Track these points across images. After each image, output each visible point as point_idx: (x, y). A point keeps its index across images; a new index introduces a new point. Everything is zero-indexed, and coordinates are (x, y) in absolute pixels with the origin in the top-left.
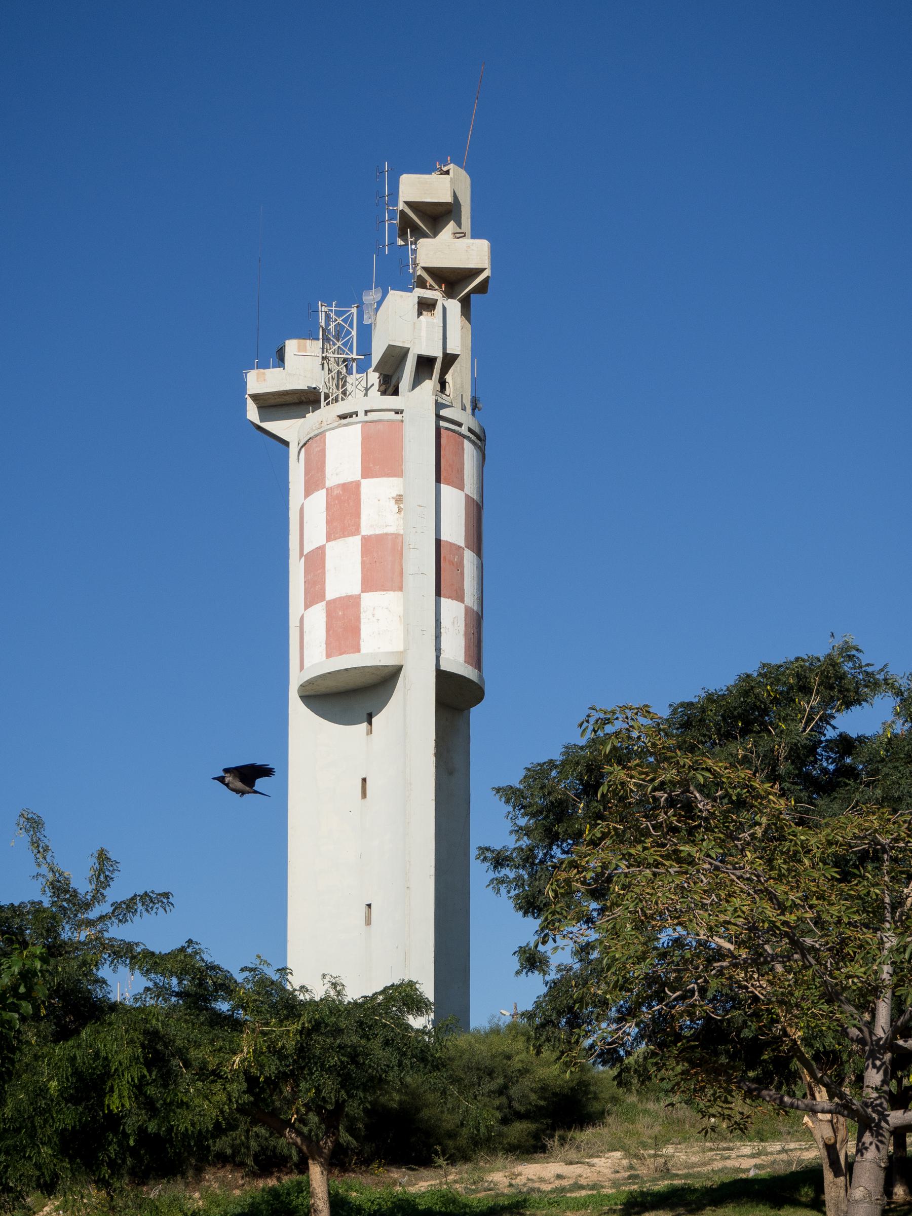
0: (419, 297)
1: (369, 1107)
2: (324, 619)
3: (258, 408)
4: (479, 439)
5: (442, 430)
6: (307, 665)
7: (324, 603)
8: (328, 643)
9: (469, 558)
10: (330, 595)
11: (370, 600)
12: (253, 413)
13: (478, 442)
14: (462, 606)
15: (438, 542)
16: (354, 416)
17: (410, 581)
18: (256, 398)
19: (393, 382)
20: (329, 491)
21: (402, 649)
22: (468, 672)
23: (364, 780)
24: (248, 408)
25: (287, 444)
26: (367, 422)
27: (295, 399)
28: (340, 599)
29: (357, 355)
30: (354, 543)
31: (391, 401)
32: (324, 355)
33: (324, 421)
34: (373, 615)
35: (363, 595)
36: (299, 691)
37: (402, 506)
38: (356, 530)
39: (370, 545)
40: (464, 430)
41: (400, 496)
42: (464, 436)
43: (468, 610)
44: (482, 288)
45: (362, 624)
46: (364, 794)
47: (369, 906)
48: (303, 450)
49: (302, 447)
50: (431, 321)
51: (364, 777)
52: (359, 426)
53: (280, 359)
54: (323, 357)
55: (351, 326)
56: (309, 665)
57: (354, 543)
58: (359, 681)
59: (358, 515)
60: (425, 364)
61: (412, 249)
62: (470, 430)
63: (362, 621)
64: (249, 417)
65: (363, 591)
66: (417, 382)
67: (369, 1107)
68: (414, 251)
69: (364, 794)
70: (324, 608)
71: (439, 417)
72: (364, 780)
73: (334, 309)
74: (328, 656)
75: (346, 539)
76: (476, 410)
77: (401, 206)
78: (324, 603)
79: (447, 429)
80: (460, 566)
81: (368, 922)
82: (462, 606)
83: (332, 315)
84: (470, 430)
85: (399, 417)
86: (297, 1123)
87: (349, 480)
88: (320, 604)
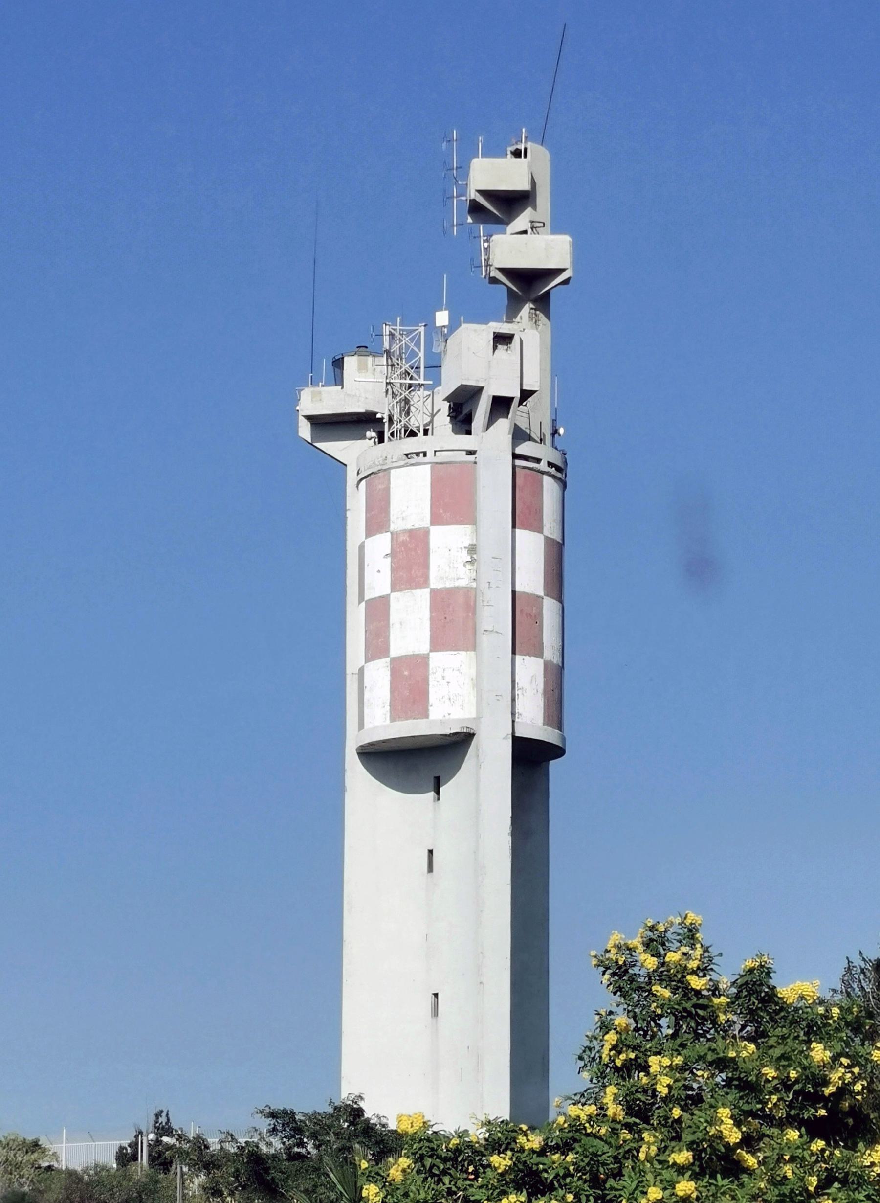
0: (494, 333)
1: (812, 1091)
2: (388, 678)
3: (312, 424)
4: (559, 470)
5: (517, 470)
6: (368, 725)
7: (388, 659)
8: (448, 397)
9: (550, 607)
10: (395, 652)
11: (439, 661)
12: (305, 431)
13: (559, 475)
14: (541, 662)
15: (514, 593)
16: (422, 455)
17: (485, 641)
18: (309, 418)
19: (465, 411)
20: (395, 536)
21: (474, 715)
22: (549, 735)
23: (431, 852)
24: (300, 424)
25: (346, 465)
26: (437, 463)
27: (355, 418)
28: (407, 657)
29: (424, 380)
30: (422, 596)
31: (465, 442)
32: (388, 381)
33: (389, 457)
34: (443, 678)
35: (431, 654)
36: (357, 750)
37: (475, 556)
38: (424, 582)
39: (398, 666)
40: (543, 466)
41: (472, 545)
42: (543, 473)
43: (547, 665)
44: (566, 282)
45: (430, 687)
46: (430, 869)
47: (436, 995)
48: (364, 481)
49: (361, 480)
50: (506, 356)
51: (431, 848)
52: (429, 466)
53: (338, 380)
54: (387, 383)
55: (418, 345)
56: (371, 726)
57: (422, 596)
58: (428, 743)
59: (426, 566)
60: (501, 405)
61: (484, 248)
62: (550, 464)
63: (430, 683)
64: (301, 434)
65: (431, 651)
66: (491, 421)
67: (812, 1091)
68: (487, 250)
69: (430, 869)
70: (389, 664)
71: (515, 456)
72: (431, 852)
73: (398, 328)
74: (393, 719)
75: (414, 591)
76: (556, 436)
77: (473, 195)
78: (388, 659)
79: (524, 468)
80: (537, 620)
81: (435, 1012)
82: (541, 662)
83: (397, 334)
84: (550, 464)
85: (471, 458)
86: (784, 1120)
87: (417, 526)
88: (383, 660)
